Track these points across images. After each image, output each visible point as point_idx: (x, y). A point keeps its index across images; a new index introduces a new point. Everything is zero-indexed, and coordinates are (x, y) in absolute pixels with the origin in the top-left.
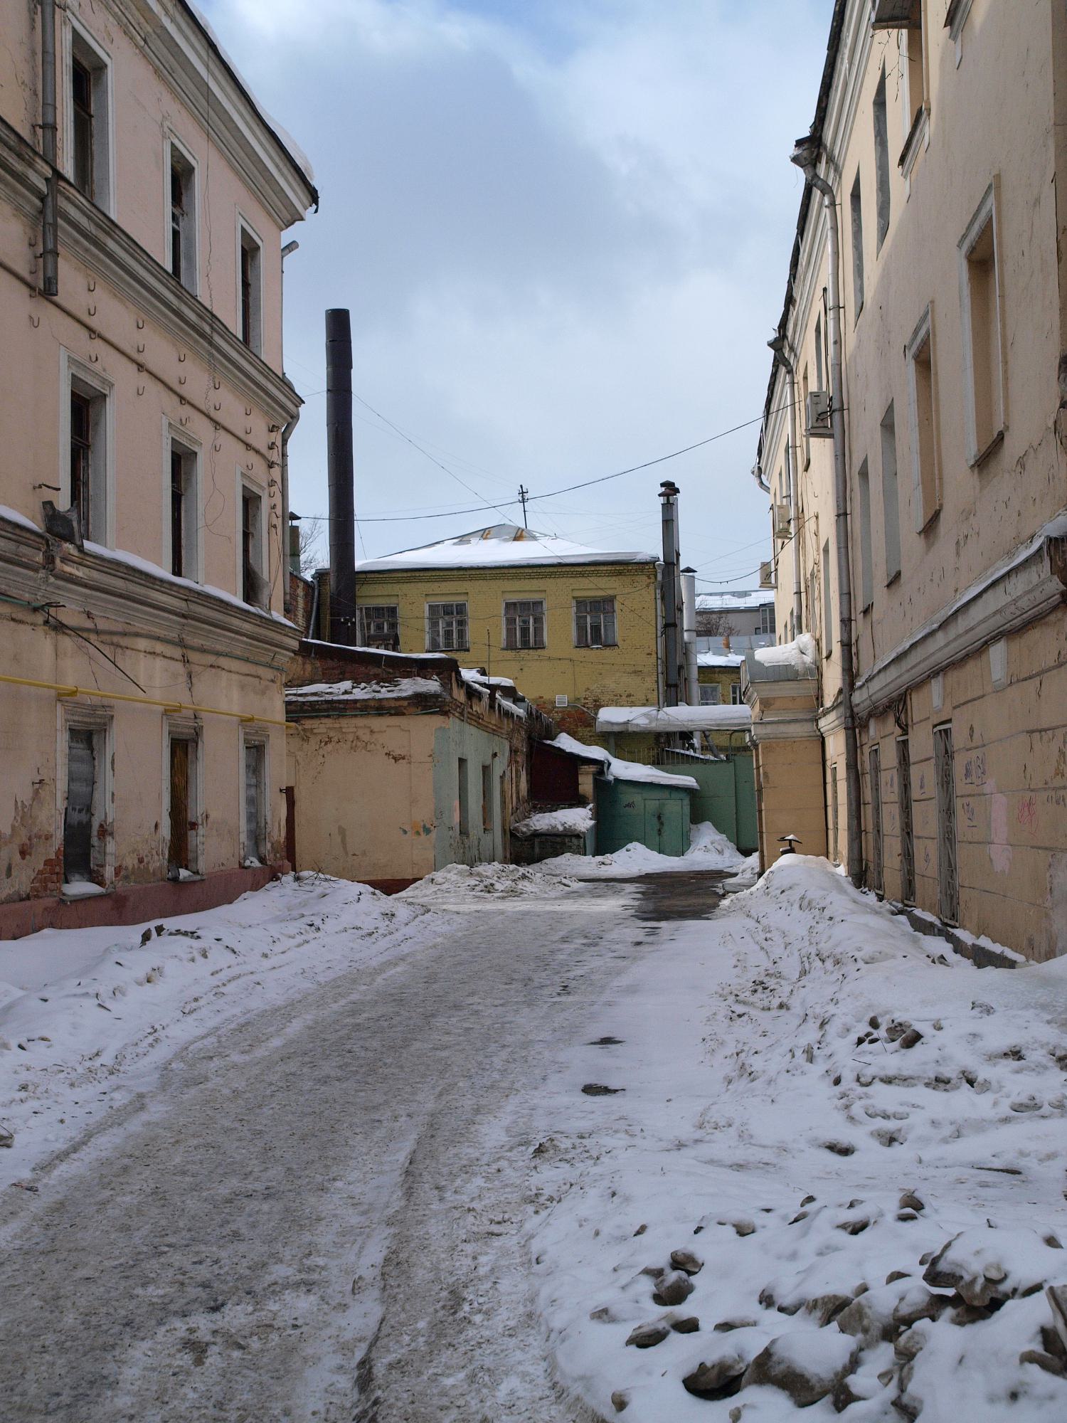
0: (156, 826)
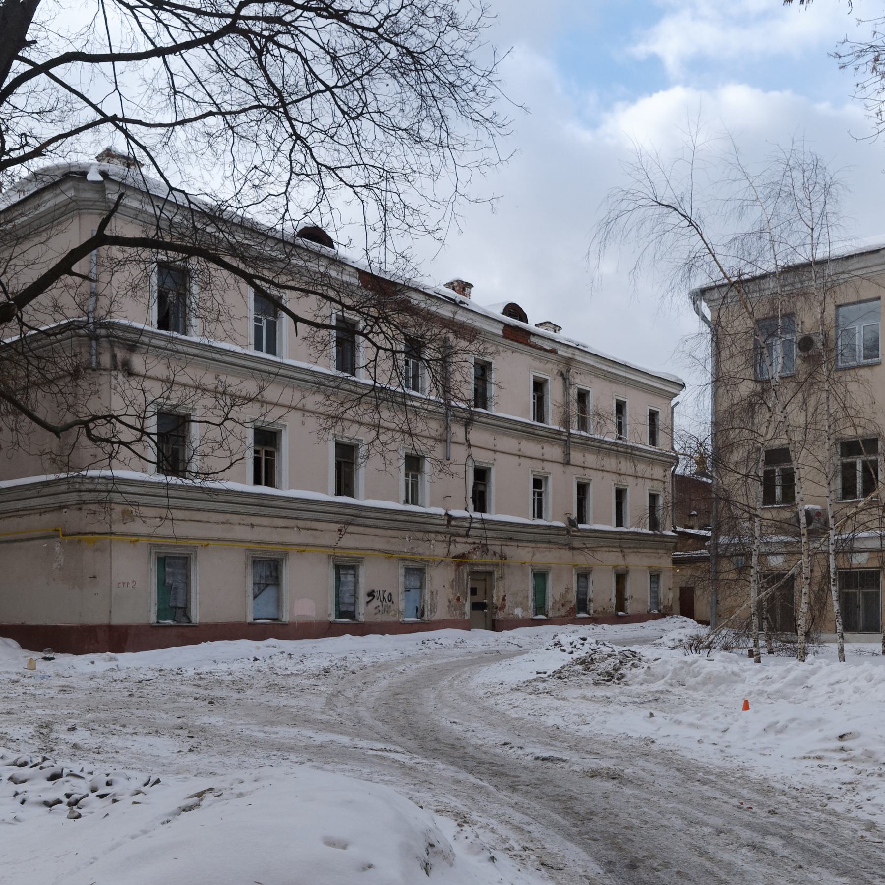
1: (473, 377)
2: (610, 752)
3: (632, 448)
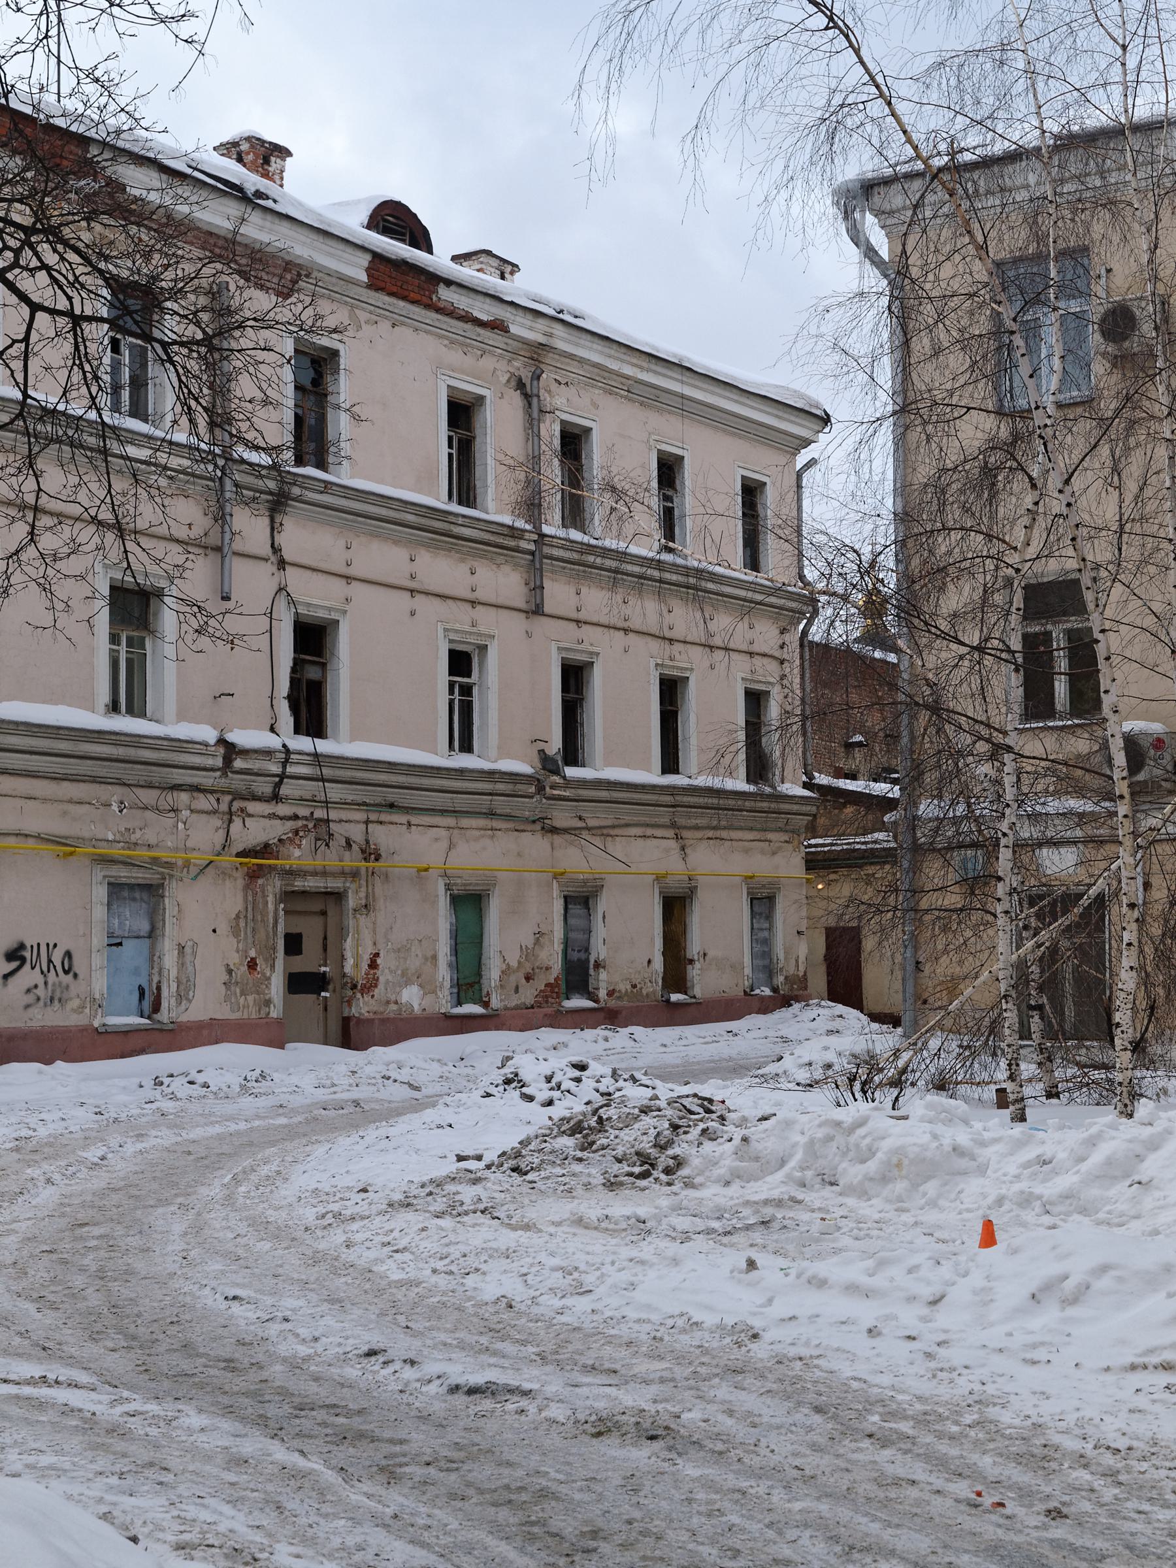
0: (649, 962)
1: (290, 390)
2: (644, 1367)
3: (699, 573)
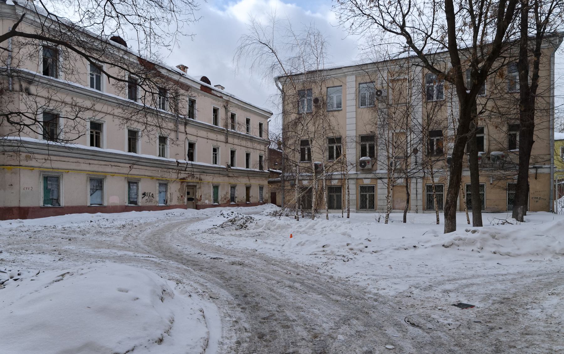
1: (188, 106)
2: (240, 255)
